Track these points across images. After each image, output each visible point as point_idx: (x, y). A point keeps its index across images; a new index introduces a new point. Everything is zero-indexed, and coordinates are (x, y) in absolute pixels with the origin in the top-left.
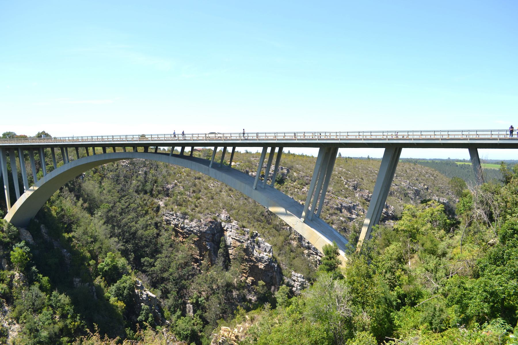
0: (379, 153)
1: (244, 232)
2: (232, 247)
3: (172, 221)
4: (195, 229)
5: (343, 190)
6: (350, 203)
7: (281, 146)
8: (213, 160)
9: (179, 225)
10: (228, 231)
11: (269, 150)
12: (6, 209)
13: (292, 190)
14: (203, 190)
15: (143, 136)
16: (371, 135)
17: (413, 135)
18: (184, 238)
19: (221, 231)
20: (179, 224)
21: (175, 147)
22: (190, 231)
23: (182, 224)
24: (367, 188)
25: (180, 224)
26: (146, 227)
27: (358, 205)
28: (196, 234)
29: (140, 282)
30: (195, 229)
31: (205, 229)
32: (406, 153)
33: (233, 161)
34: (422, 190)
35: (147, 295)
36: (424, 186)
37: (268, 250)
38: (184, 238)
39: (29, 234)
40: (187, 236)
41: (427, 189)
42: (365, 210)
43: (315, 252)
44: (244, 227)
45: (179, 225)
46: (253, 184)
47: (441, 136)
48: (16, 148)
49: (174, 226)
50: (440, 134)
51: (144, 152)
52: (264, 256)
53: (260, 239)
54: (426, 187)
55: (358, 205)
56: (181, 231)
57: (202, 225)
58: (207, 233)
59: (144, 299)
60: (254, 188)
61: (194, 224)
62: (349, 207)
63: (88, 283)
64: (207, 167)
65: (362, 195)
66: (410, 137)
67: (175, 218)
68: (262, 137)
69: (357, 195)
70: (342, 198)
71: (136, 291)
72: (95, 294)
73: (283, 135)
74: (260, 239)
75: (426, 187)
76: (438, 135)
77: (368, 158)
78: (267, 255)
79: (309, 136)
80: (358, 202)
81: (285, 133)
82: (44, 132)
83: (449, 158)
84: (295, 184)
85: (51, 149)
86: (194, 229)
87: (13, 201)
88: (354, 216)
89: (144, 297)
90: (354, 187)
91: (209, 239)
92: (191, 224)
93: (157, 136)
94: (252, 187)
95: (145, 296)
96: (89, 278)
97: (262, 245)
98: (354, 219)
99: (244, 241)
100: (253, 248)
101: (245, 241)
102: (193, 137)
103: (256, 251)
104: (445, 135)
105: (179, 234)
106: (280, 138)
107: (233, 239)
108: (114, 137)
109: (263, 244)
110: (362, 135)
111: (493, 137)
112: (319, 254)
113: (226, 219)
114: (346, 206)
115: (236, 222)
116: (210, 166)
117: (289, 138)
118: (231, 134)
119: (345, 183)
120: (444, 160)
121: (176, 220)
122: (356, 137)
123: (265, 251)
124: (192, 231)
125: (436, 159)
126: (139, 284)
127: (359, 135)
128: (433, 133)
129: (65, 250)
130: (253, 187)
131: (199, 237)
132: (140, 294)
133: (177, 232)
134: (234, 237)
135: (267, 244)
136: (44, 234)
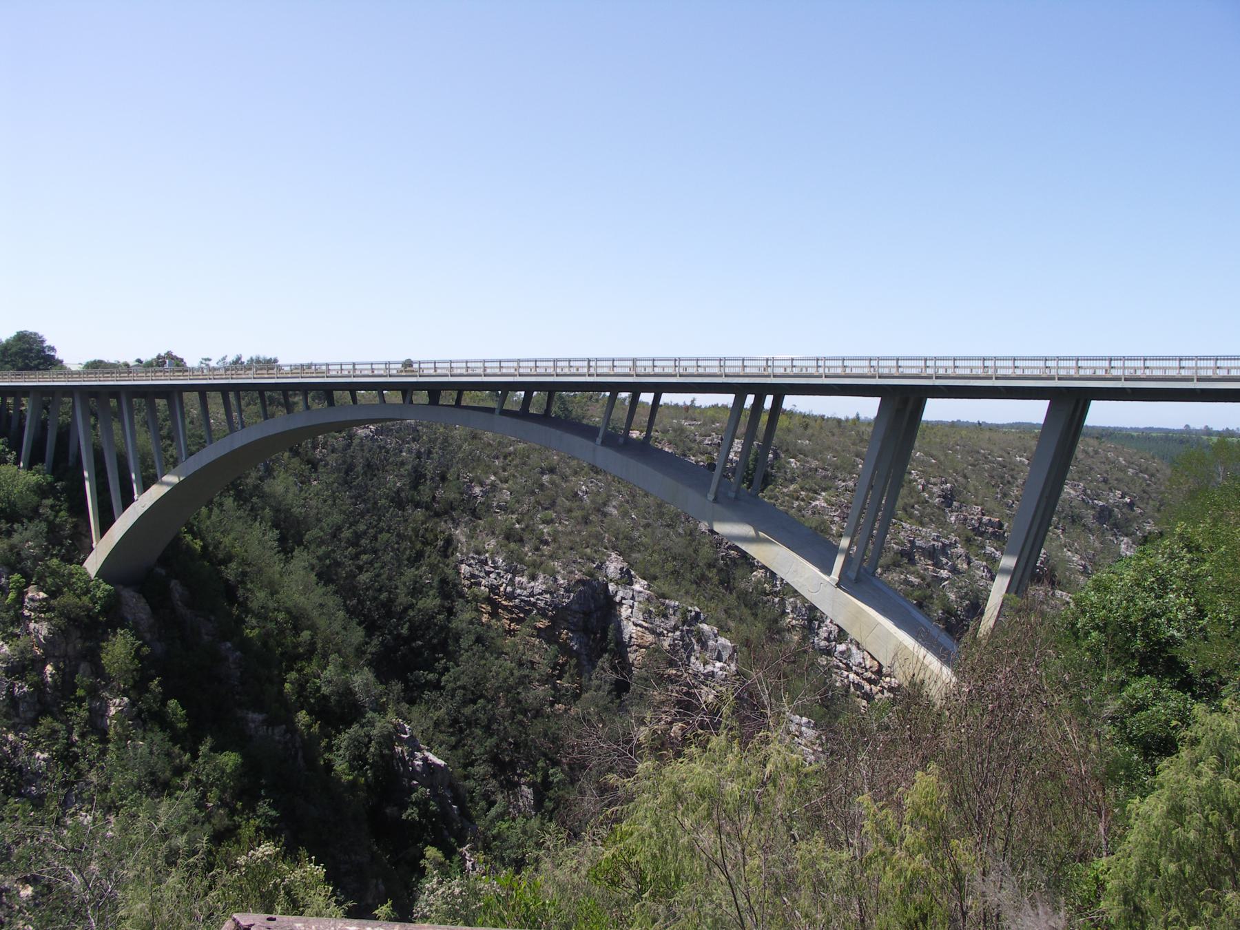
0: (1035, 412)
1: (666, 609)
2: (635, 647)
3: (483, 578)
4: (541, 600)
5: (916, 506)
6: (934, 539)
7: (780, 391)
8: (608, 423)
9: (502, 589)
10: (624, 606)
11: (750, 399)
12: (88, 540)
13: (786, 503)
14: (561, 500)
15: (408, 364)
16: (955, 367)
17: (1124, 368)
18: (512, 620)
19: (609, 606)
20: (501, 585)
21: (642, 394)
22: (528, 603)
23: (507, 585)
24: (979, 502)
25: (504, 585)
26: (417, 590)
27: (953, 545)
28: (543, 613)
29: (407, 727)
30: (541, 600)
31: (566, 600)
32: (1100, 414)
33: (633, 425)
34: (1118, 507)
35: (425, 759)
36: (1123, 497)
37: (725, 656)
38: (512, 620)
39: (143, 603)
40: (522, 615)
41: (1131, 505)
42: (971, 557)
43: (844, 661)
44: (664, 596)
45: (502, 589)
46: (709, 487)
47: (827, 370)
48: (115, 391)
49: (487, 590)
50: (1194, 365)
51: (430, 403)
52: (716, 670)
53: (705, 627)
54: (1129, 501)
55: (953, 545)
56: (505, 603)
57: (558, 590)
58: (571, 610)
59: (418, 769)
60: (711, 497)
61: (538, 586)
62: (932, 550)
63: (284, 726)
64: (592, 444)
65: (965, 520)
66: (1114, 373)
67: (493, 570)
68: (733, 367)
69: (953, 519)
70: (914, 527)
71: (399, 749)
72: (300, 754)
73: (610, 363)
74: (705, 627)
75: (1127, 500)
76: (1189, 368)
77: (979, 423)
78: (722, 669)
79: (861, 368)
80: (953, 538)
81: (926, 360)
82: (169, 355)
83: (1187, 426)
84: (792, 487)
85: (199, 394)
86: (538, 599)
87: (106, 523)
88: (944, 573)
89: (418, 765)
90: (944, 497)
91: (575, 625)
92: (530, 585)
93: (369, 367)
94: (706, 496)
95: (420, 763)
96: (282, 714)
97: (711, 643)
98: (946, 580)
99: (665, 632)
100: (688, 648)
101: (669, 632)
102: (435, 368)
103: (697, 659)
104: (1170, 368)
105: (500, 610)
106: (779, 373)
107: (636, 625)
108: (357, 367)
109: (713, 639)
110: (992, 367)
111: (1184, 373)
112: (854, 668)
113: (619, 576)
114: (924, 545)
115: (646, 583)
116: (599, 440)
117: (940, 374)
118: (500, 362)
119: (920, 487)
120: (1173, 431)
121: (493, 576)
122: (785, 370)
123: (719, 659)
124: (535, 604)
125: (1151, 429)
126: (406, 733)
127: (793, 366)
128: (1178, 362)
129: (229, 644)
130: (708, 495)
131: (551, 619)
132: (407, 758)
133: (495, 605)
134: (640, 622)
135: (722, 640)
136: (179, 603)
